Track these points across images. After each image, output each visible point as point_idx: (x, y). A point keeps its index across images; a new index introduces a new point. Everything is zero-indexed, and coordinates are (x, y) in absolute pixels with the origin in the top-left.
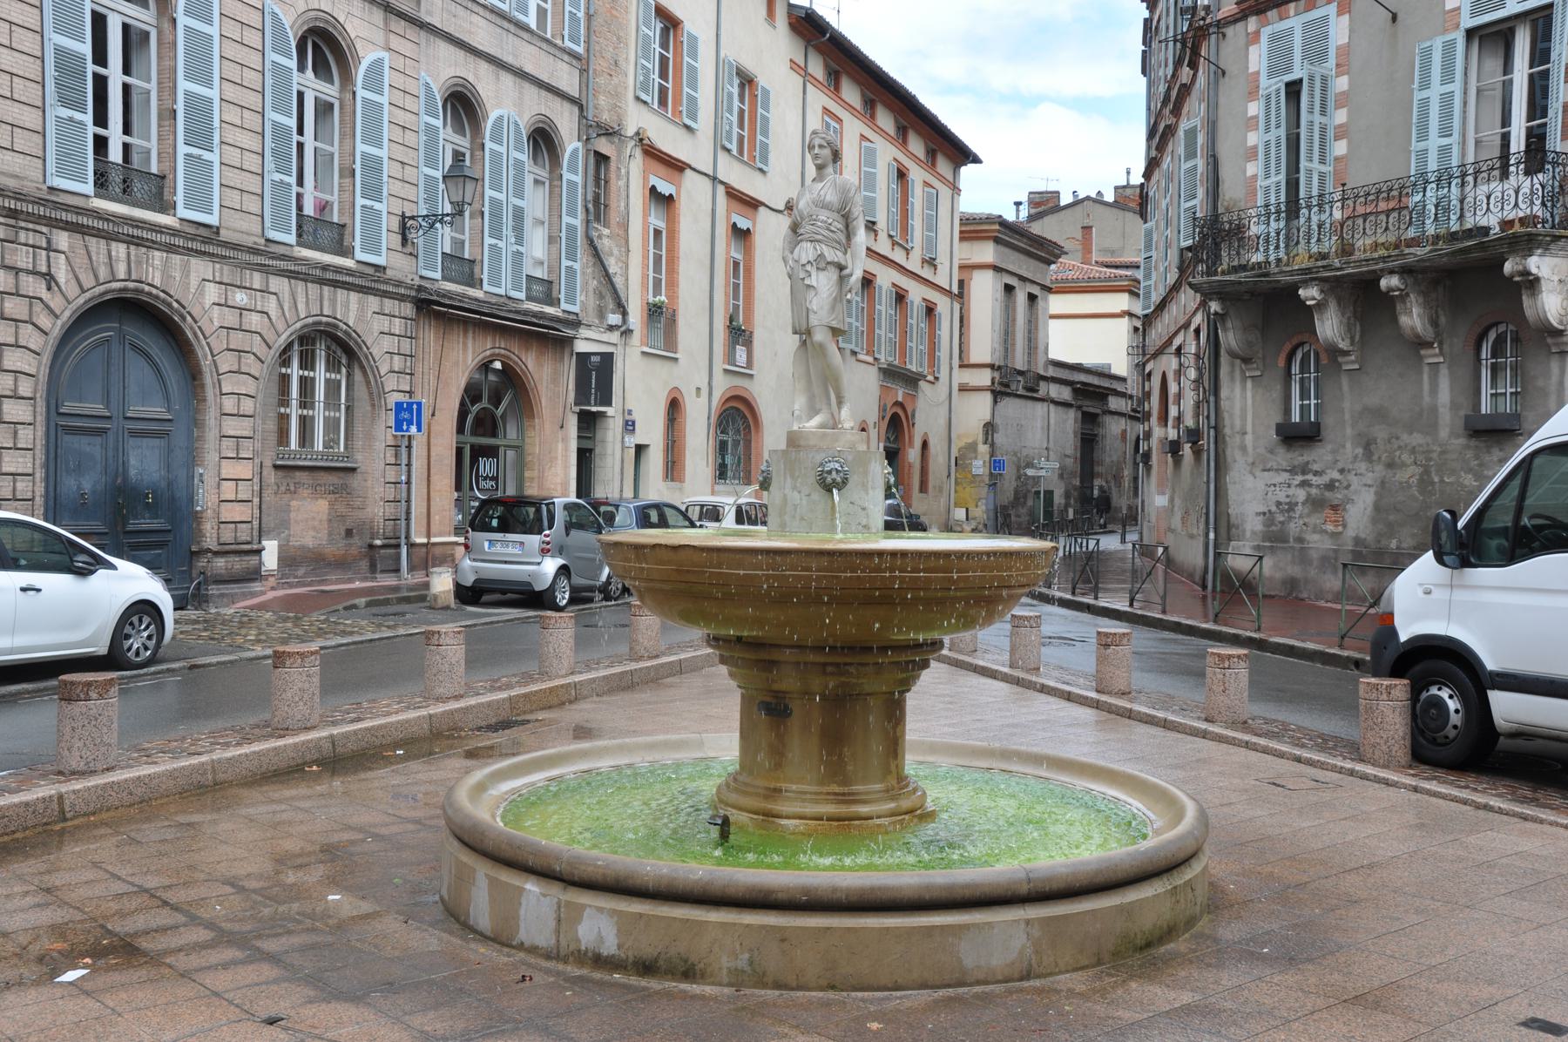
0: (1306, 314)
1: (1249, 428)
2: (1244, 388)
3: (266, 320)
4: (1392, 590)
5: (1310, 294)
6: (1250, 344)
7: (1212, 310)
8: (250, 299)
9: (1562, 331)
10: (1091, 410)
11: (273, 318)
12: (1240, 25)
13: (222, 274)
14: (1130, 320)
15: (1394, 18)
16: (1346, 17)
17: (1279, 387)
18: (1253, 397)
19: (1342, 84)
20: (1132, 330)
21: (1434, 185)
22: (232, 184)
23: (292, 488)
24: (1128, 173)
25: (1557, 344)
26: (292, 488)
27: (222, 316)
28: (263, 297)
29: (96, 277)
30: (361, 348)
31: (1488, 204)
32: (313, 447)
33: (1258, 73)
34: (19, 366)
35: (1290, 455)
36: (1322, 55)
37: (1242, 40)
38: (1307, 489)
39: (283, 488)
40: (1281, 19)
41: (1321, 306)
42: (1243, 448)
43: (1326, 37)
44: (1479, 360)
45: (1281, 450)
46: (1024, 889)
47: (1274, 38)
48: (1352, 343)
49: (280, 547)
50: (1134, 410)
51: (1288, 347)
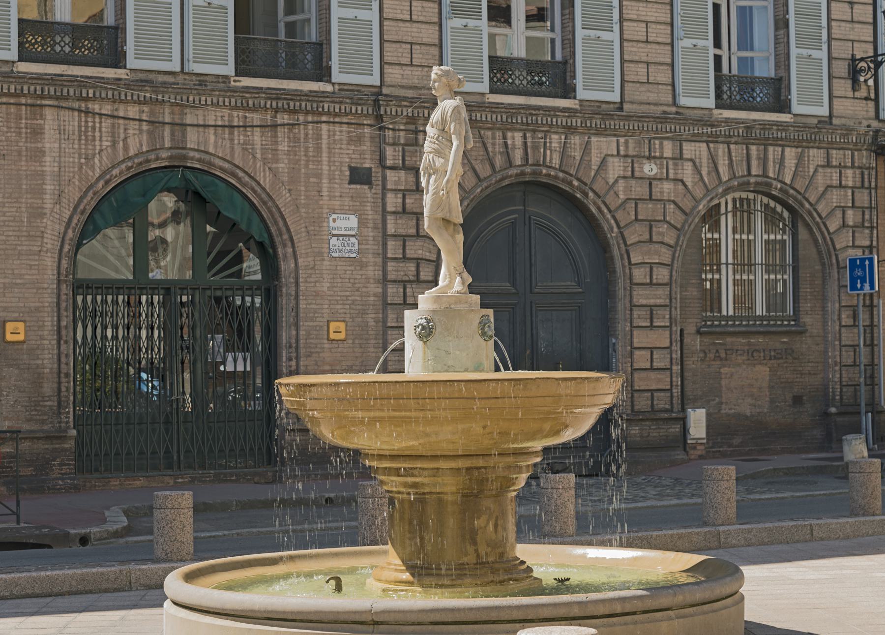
3: (680, 187)
8: (661, 168)
11: (689, 185)
13: (627, 147)
22: (636, 58)
23: (723, 355)
26: (723, 355)
27: (628, 189)
28: (675, 165)
29: (493, 166)
30: (802, 205)
32: (720, 311)
34: (420, 253)
39: (711, 355)
49: (708, 415)
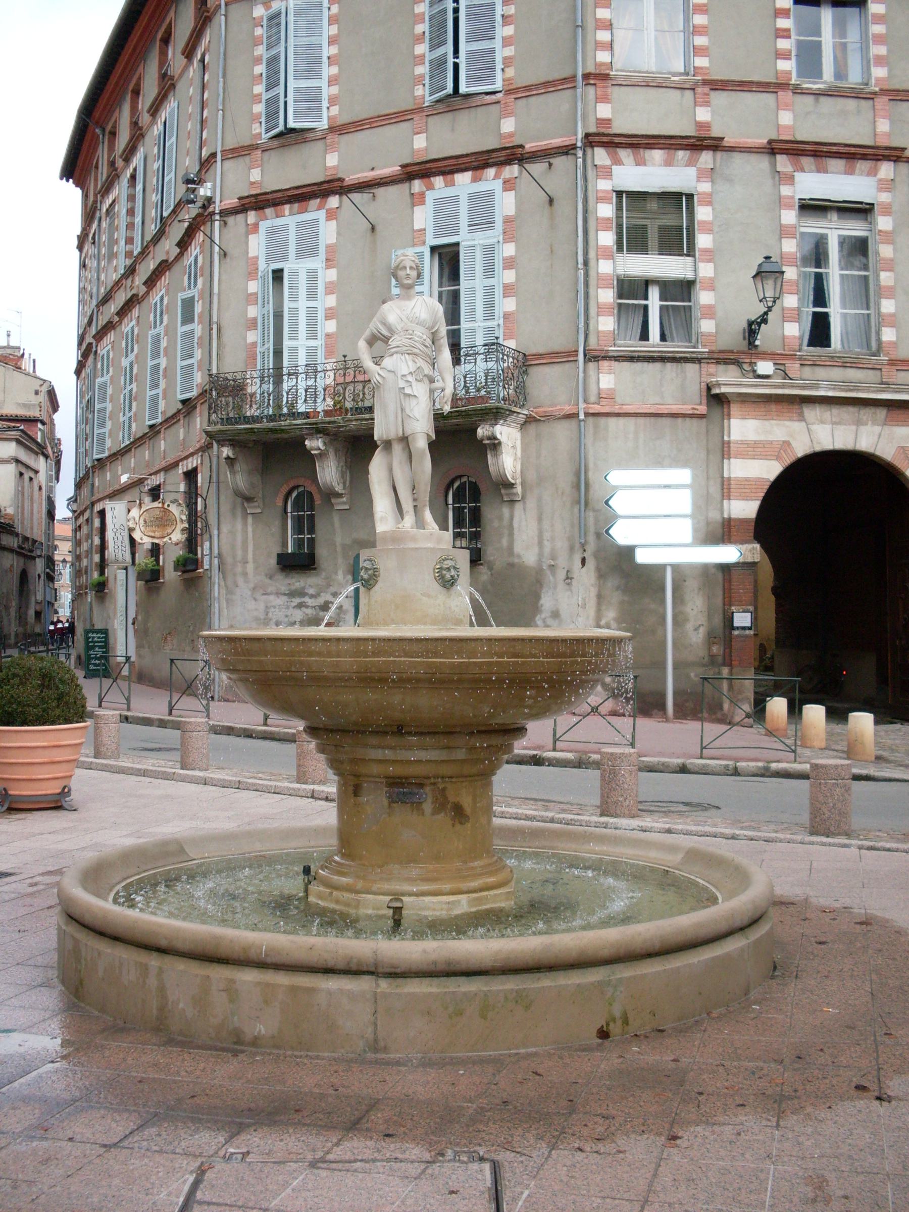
0: (309, 459)
2: (245, 524)
4: (249, 705)
5: (315, 444)
6: (253, 486)
12: (240, 217)
14: (17, 466)
15: (373, 229)
16: (334, 223)
17: (277, 523)
18: (253, 531)
20: (18, 474)
21: (304, 376)
24: (9, 335)
25: (508, 495)
33: (257, 258)
35: (288, 581)
37: (242, 229)
38: (304, 609)
40: (277, 216)
41: (322, 455)
42: (245, 574)
43: (317, 236)
44: (447, 505)
45: (280, 577)
46: (657, 946)
47: (272, 232)
48: (344, 488)
50: (20, 547)
51: (285, 489)
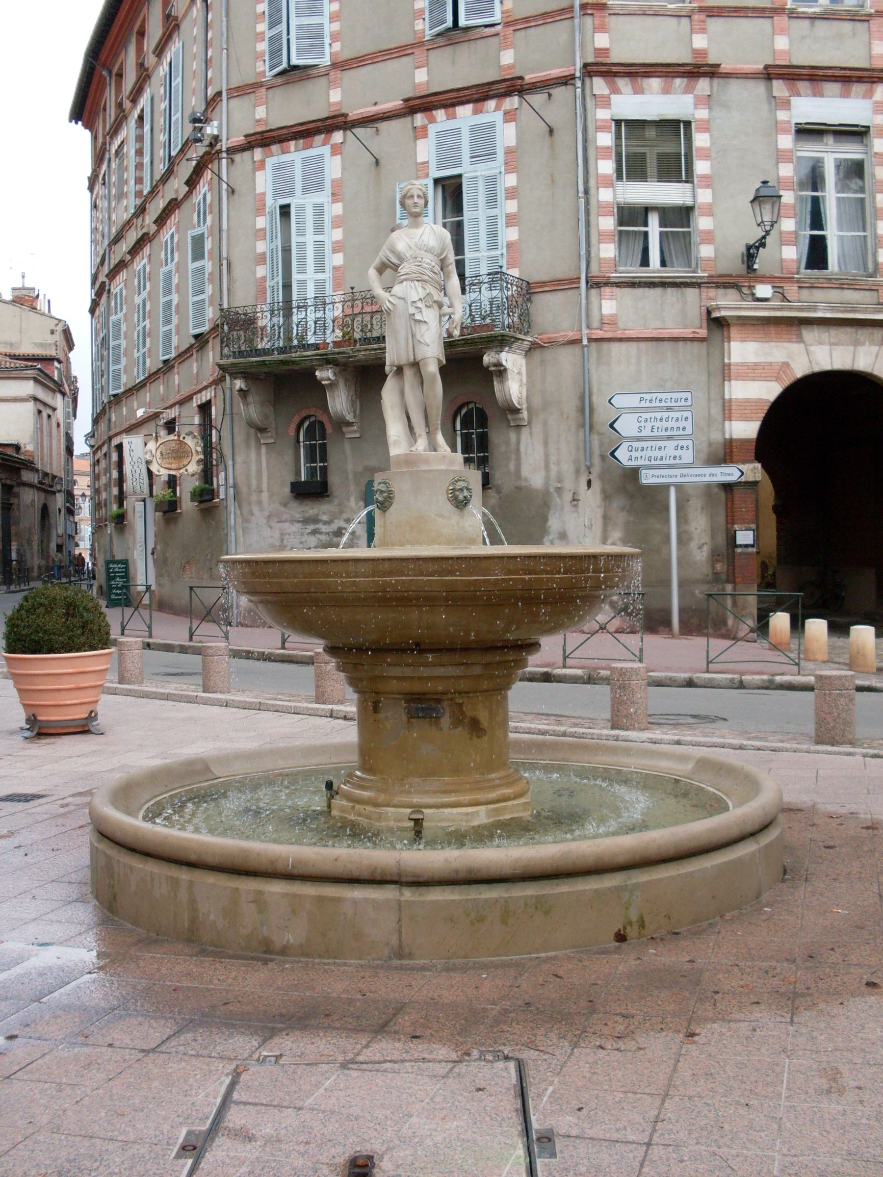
0: (319, 390)
1: (264, 486)
2: (259, 454)
5: (325, 375)
7: (237, 387)
9: (519, 410)
10: (8, 482)
12: (247, 154)
14: (35, 404)
15: (377, 163)
16: (339, 157)
18: (268, 461)
19: (511, 180)
21: (313, 308)
25: (514, 420)
31: (315, 328)
33: (264, 194)
35: (302, 508)
36: (490, 155)
37: (249, 166)
38: (318, 536)
40: (283, 153)
41: (333, 385)
43: (322, 171)
44: (455, 431)
45: (294, 504)
47: (278, 168)
48: (355, 417)
50: (40, 483)
51: (297, 420)
